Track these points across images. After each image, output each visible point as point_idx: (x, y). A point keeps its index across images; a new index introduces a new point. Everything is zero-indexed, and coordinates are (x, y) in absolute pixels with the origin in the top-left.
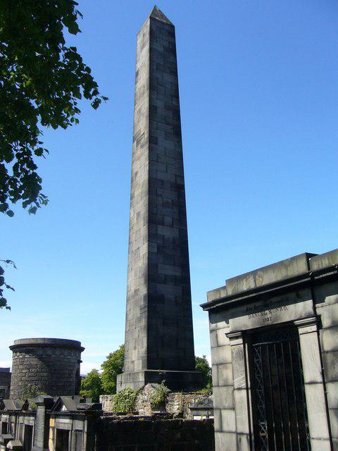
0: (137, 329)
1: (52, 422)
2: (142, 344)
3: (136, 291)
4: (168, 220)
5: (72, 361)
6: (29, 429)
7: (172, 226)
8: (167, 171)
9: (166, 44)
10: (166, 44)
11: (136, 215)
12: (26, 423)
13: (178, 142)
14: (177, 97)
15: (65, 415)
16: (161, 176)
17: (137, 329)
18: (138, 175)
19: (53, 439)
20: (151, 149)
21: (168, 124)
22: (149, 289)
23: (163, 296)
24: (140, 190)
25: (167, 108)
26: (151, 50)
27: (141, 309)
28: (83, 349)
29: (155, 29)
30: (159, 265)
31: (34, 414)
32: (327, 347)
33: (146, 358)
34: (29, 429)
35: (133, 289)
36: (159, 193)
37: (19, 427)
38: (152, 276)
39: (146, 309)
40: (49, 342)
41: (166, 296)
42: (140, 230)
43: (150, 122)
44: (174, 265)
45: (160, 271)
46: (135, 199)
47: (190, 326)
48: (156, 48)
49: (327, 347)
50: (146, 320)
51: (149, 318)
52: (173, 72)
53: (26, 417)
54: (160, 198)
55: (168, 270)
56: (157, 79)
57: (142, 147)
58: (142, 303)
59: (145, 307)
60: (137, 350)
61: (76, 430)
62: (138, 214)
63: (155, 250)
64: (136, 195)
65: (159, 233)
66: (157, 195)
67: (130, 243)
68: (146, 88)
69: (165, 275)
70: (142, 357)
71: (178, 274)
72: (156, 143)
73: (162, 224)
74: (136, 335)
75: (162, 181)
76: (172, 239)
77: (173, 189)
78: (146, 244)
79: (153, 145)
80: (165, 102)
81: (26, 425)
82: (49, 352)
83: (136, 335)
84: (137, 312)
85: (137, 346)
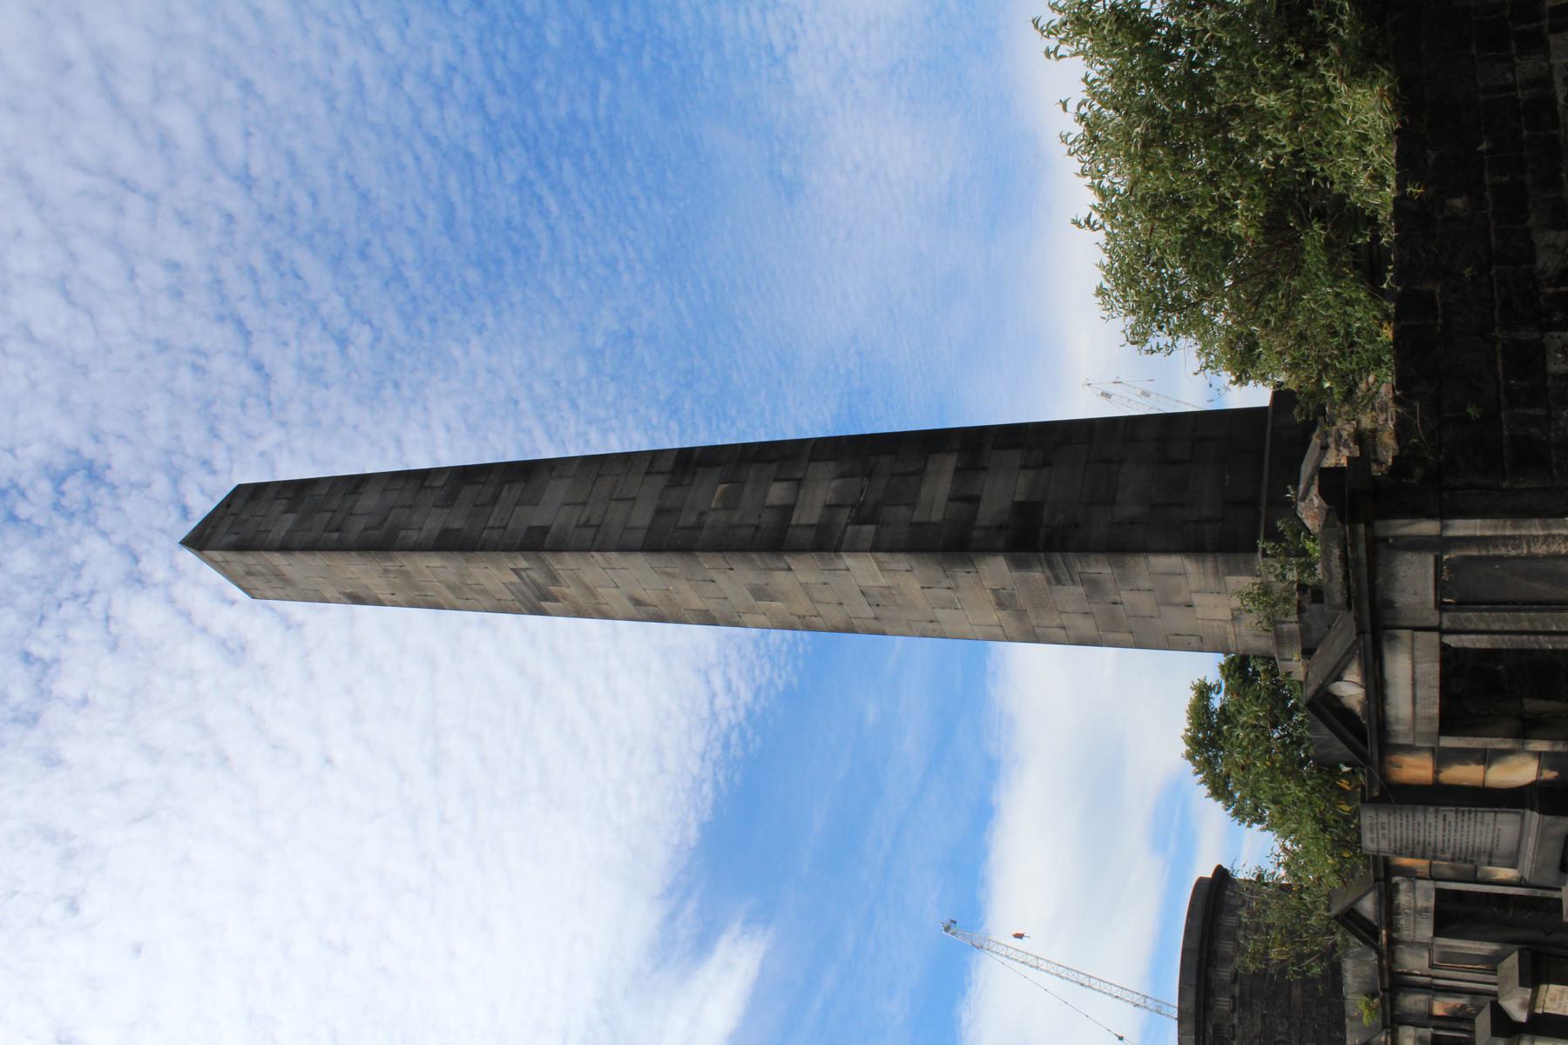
0: (1125, 596)
1: (1415, 769)
2: (1174, 574)
4: (778, 493)
6: (1453, 914)
7: (799, 483)
8: (633, 499)
9: (281, 505)
10: (281, 505)
11: (764, 604)
12: (1425, 931)
13: (553, 469)
15: (1376, 686)
16: (642, 516)
17: (1125, 596)
18: (640, 594)
19: (1487, 758)
20: (559, 547)
21: (495, 499)
22: (989, 550)
25: (449, 501)
26: (285, 548)
27: (1059, 581)
28: (1221, 872)
29: (234, 538)
30: (916, 518)
31: (1384, 875)
33: (1221, 558)
34: (1453, 914)
35: (996, 616)
36: (692, 520)
37: (1449, 976)
38: (953, 544)
39: (1057, 558)
41: (1019, 498)
42: (805, 587)
43: (481, 550)
44: (920, 473)
45: (937, 516)
46: (711, 605)
47: (1194, 641)
48: (283, 533)
50: (1092, 557)
51: (1085, 548)
52: (357, 487)
53: (1405, 934)
54: (709, 519)
55: (937, 491)
56: (366, 529)
57: (554, 579)
58: (1037, 575)
59: (1051, 565)
60: (1196, 599)
61: (1441, 606)
62: (760, 593)
63: (868, 530)
64: (698, 604)
65: (815, 520)
66: (699, 526)
67: (851, 629)
69: (950, 499)
70: (1216, 573)
71: (950, 462)
72: (545, 530)
73: (787, 510)
74: (1144, 602)
75: (660, 511)
76: (838, 482)
77: (686, 481)
78: (849, 560)
79: (548, 543)
80: (435, 506)
81: (1436, 934)
82: (1225, 973)
83: (1144, 602)
84: (1070, 595)
85: (1179, 599)
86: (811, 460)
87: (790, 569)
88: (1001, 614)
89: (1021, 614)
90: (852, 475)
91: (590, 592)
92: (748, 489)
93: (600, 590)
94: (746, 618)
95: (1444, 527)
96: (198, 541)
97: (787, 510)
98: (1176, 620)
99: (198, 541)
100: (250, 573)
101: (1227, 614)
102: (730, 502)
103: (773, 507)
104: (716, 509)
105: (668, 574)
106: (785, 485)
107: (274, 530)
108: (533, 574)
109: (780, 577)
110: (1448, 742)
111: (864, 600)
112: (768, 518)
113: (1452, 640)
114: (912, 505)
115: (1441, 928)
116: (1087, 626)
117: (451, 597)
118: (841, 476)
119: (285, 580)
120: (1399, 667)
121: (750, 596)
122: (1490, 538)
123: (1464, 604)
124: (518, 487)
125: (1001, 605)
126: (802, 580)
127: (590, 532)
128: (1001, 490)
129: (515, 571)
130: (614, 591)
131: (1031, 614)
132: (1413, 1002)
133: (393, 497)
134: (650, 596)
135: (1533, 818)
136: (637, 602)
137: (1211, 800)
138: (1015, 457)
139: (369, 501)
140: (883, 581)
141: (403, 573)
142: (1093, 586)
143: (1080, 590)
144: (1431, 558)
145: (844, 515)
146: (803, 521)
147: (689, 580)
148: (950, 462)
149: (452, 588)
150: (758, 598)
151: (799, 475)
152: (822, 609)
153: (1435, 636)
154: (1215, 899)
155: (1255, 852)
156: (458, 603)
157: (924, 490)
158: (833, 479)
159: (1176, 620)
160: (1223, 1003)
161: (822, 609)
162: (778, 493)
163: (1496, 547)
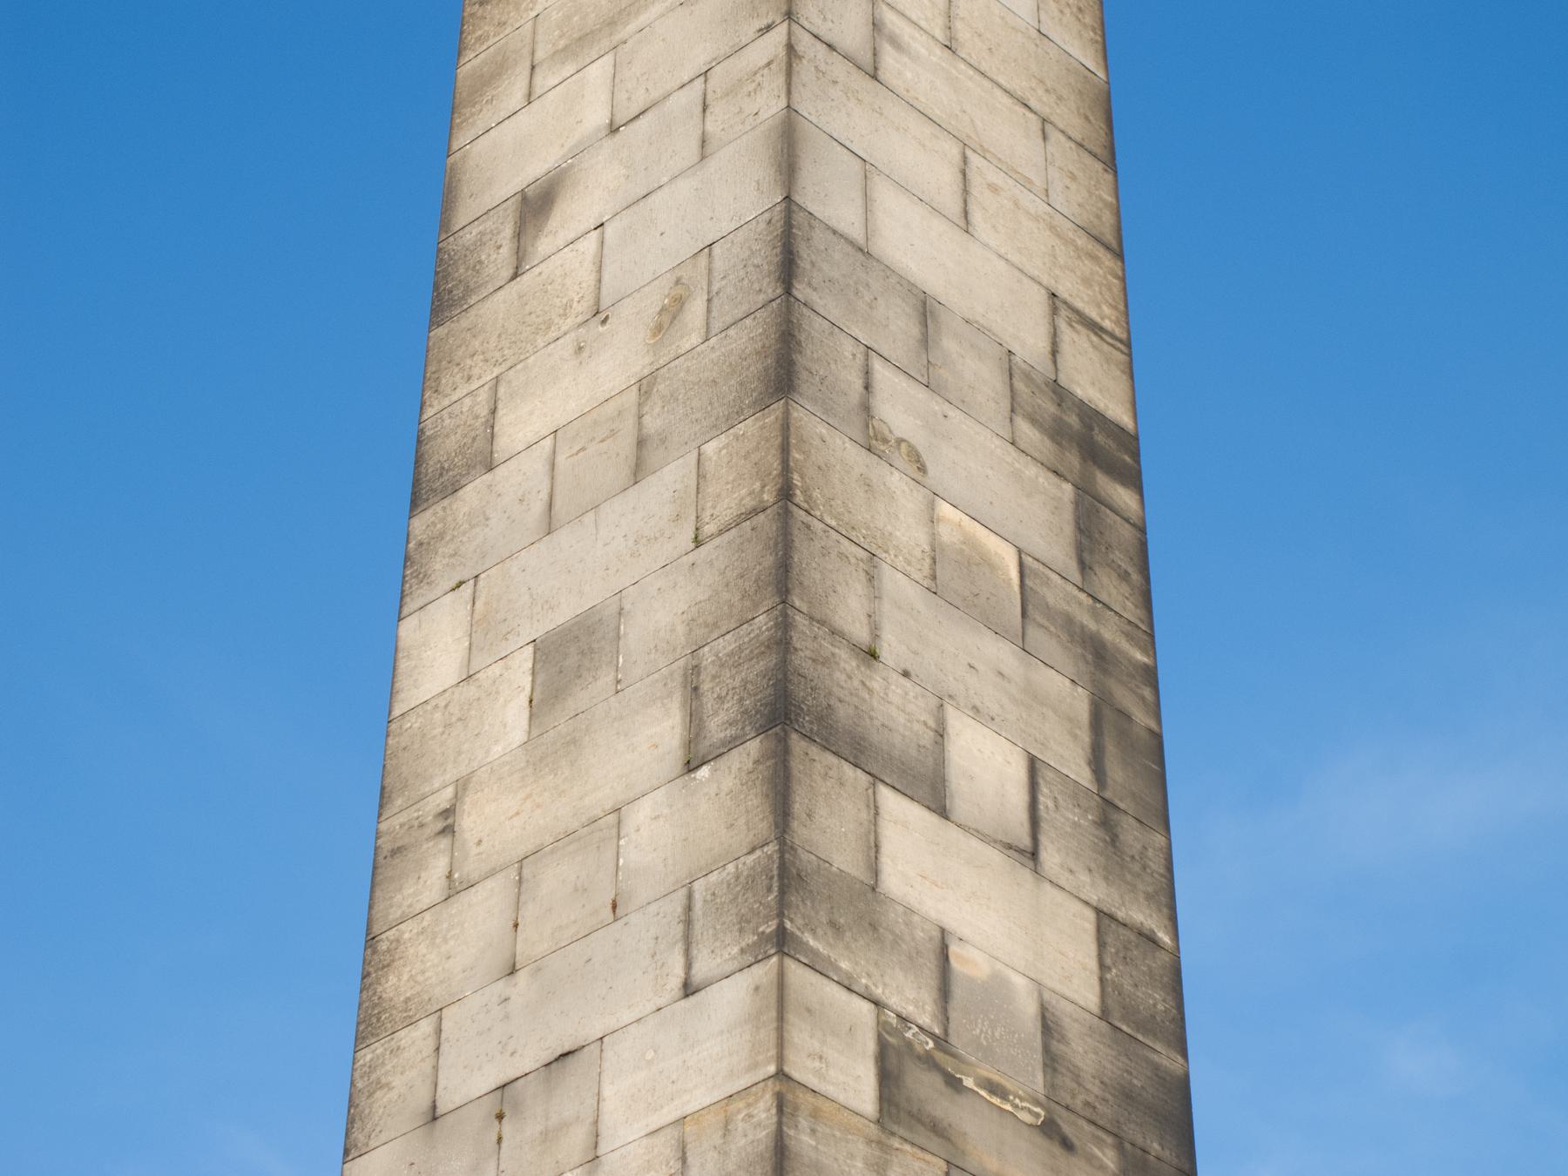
4: (987, 765)
63: (855, 1084)
65: (893, 881)
66: (873, 441)
73: (934, 793)
75: (926, 311)
77: (1026, 430)
86: (1104, 919)
87: (690, 767)
90: (1052, 1061)
92: (1002, 653)
93: (598, 72)
97: (934, 793)
102: (949, 577)
103: (941, 733)
104: (932, 520)
105: (673, 310)
106: (1018, 797)
109: (663, 730)
111: (530, 1058)
112: (893, 708)
118: (1048, 1025)
121: (564, 613)
126: (640, 815)
130: (596, 116)
145: (911, 997)
146: (890, 836)
147: (645, 387)
150: (1130, 441)
151: (1051, 857)
158: (1039, 985)
161: (485, 908)
162: (987, 765)
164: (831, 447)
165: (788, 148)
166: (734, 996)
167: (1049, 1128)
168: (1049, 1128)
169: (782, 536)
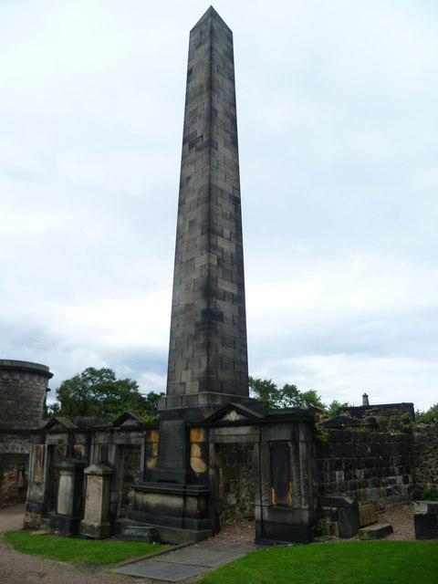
3: (189, 307)
4: (227, 232)
5: (41, 388)
10: (226, 48)
11: (188, 224)
14: (234, 105)
15: (88, 451)
17: (191, 348)
18: (192, 180)
21: (226, 131)
23: (222, 314)
24: (195, 196)
29: (215, 29)
32: (112, 500)
35: (182, 303)
40: (10, 364)
42: (195, 239)
47: (176, 308)
49: (112, 500)
60: (189, 371)
62: (192, 223)
65: (219, 244)
68: (205, 88)
71: (235, 292)
83: (189, 353)
84: (192, 329)
85: (189, 365)
88: (183, 306)
89: (183, 312)
91: (193, 162)
94: (182, 217)
95: (302, 442)
96: (212, 13)
98: (181, 365)
99: (212, 13)
100: (201, 33)
101: (183, 380)
102: (224, 215)
107: (212, 46)
108: (200, 143)
109: (199, 231)
110: (211, 446)
112: (218, 228)
113: (257, 445)
114: (223, 278)
115: (120, 447)
116: (179, 333)
117: (190, 110)
119: (200, 44)
120: (244, 430)
122: (298, 454)
123: (271, 450)
124: (230, 140)
125: (187, 306)
127: (216, 165)
128: (225, 307)
129: (202, 136)
131: (184, 316)
132: (81, 438)
133: (227, 92)
134: (191, 183)
135: (184, 471)
136: (188, 179)
137: (268, 380)
138: (236, 313)
139: (227, 83)
140: (197, 266)
141: (201, 93)
142: (195, 337)
143: (193, 332)
144: (289, 439)
145: (220, 255)
148: (235, 292)
149: (195, 111)
152: (185, 244)
153: (258, 440)
154: (43, 373)
155: (55, 383)
156: (188, 112)
157: (226, 282)
159: (181, 365)
160: (6, 376)
161: (185, 244)
162: (227, 232)
163: (295, 462)
164: (214, 206)
165: (210, 177)
166: (205, 256)
167: (232, 264)
168: (232, 264)
169: (209, 215)
